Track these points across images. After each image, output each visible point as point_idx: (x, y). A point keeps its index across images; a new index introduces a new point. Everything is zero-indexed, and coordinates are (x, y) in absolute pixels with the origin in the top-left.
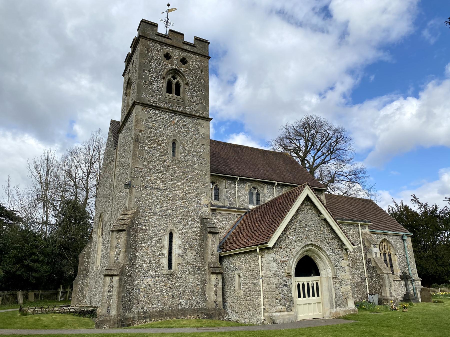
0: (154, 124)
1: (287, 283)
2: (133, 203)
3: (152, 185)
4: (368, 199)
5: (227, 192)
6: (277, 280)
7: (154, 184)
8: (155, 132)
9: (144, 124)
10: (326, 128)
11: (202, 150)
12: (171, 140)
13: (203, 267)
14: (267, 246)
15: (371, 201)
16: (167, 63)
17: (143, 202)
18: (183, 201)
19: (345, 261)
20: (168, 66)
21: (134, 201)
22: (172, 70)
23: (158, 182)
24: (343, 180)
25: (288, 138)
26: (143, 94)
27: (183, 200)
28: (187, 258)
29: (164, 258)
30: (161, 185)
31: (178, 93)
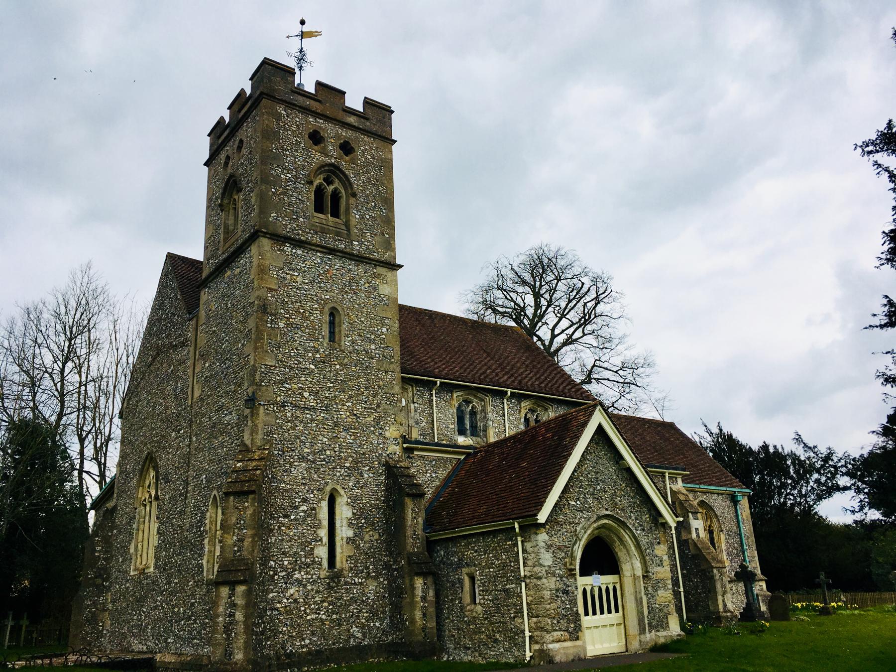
0: (295, 277)
1: (570, 588)
2: (260, 436)
3: (294, 399)
4: (659, 418)
5: (415, 411)
6: (551, 583)
7: (299, 399)
8: (296, 293)
9: (275, 276)
10: (577, 270)
11: (384, 330)
12: (326, 310)
13: (395, 562)
14: (537, 519)
15: (671, 426)
16: (316, 152)
17: (279, 434)
18: (353, 433)
19: (662, 546)
20: (317, 158)
21: (262, 432)
22: (326, 165)
23: (306, 394)
24: (608, 379)
25: (499, 288)
26: (272, 215)
27: (353, 431)
28: (363, 546)
29: (322, 545)
30: (312, 401)
31: (335, 213)
